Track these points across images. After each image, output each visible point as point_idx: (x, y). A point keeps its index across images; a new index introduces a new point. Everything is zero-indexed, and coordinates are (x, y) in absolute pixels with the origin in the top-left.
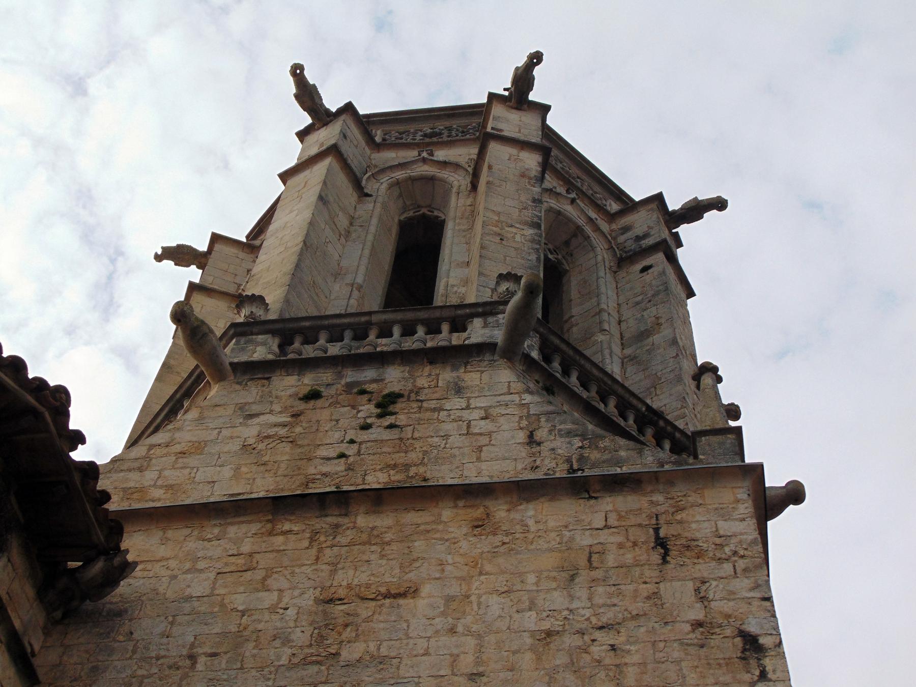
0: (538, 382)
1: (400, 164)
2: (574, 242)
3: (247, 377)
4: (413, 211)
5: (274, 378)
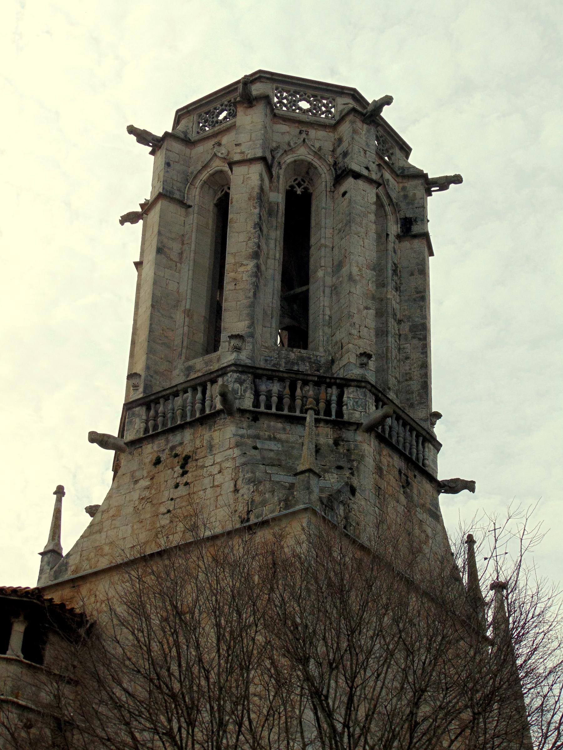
0: (248, 418)
1: (203, 167)
2: (311, 173)
3: (133, 448)
4: (220, 192)
5: (143, 447)
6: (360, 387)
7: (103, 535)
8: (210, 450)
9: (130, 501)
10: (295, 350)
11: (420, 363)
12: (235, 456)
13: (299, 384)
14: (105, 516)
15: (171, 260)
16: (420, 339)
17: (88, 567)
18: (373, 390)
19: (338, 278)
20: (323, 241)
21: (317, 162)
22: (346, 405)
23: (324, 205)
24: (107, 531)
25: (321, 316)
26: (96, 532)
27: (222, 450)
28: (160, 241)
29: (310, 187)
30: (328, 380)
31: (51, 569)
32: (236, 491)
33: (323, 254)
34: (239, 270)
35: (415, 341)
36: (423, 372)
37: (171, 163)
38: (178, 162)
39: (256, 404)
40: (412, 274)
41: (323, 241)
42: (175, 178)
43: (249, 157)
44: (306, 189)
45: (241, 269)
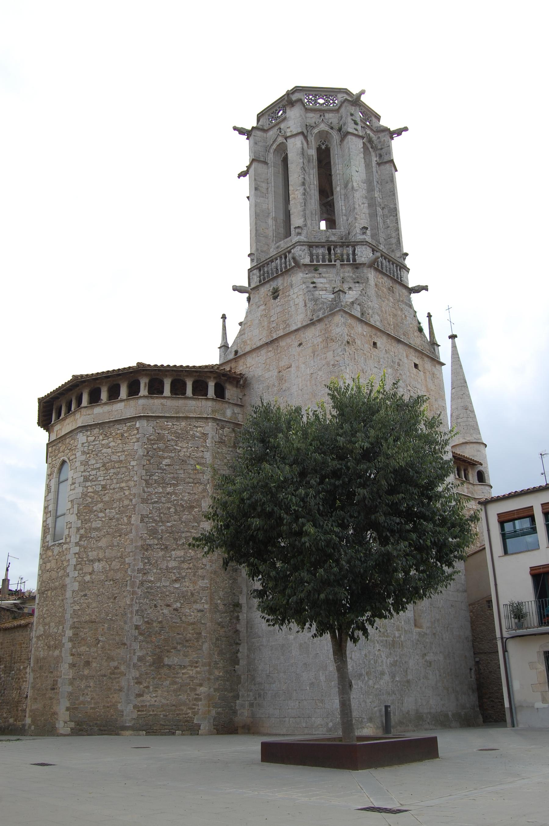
6: (363, 245)
7: (246, 335)
9: (256, 317)
14: (246, 326)
22: (357, 255)
23: (336, 153)
27: (297, 286)
32: (305, 306)
36: (397, 233)
40: (387, 183)
44: (327, 145)
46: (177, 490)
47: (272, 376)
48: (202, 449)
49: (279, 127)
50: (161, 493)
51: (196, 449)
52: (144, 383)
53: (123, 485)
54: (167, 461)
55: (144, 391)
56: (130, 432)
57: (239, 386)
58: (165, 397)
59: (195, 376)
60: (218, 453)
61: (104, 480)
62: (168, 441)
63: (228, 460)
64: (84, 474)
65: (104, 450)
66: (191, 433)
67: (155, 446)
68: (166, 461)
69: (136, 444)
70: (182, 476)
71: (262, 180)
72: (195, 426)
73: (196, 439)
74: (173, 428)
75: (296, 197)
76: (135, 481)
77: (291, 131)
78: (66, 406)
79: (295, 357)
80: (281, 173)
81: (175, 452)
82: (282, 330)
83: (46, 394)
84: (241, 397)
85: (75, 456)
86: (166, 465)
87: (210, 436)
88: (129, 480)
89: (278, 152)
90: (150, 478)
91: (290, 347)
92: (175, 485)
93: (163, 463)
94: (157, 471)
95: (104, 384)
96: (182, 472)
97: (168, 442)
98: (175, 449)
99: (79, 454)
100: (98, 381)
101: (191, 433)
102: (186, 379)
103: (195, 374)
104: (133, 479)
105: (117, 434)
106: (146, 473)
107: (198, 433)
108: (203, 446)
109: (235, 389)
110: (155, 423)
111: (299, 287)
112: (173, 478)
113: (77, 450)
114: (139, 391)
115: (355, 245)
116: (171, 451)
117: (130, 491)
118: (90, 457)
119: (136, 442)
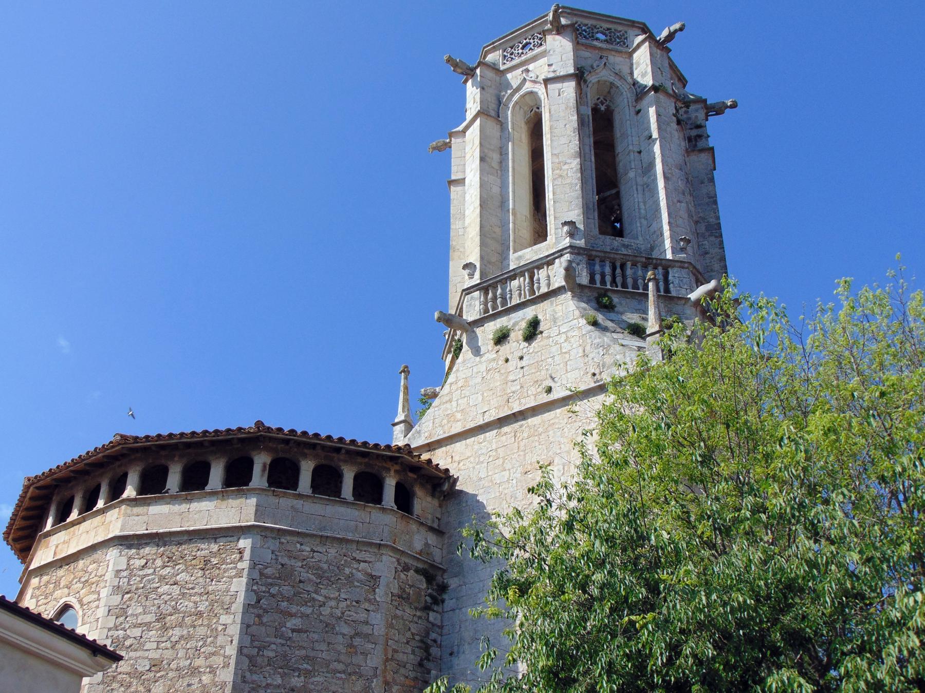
2: (612, 91)
6: (683, 268)
7: (454, 404)
8: (555, 322)
9: (477, 373)
10: (617, 238)
11: (719, 257)
12: (580, 325)
13: (629, 264)
14: (454, 387)
15: (493, 167)
16: (716, 237)
17: (442, 432)
18: (694, 271)
19: (649, 178)
20: (631, 147)
21: (618, 83)
22: (673, 283)
23: (628, 117)
24: (457, 400)
25: (637, 210)
26: (446, 402)
27: (566, 321)
28: (481, 151)
29: (611, 104)
30: (654, 261)
31: (405, 437)
32: (585, 355)
33: (632, 157)
34: (563, 168)
35: (712, 239)
36: (722, 264)
37: (485, 87)
38: (491, 87)
39: (592, 280)
40: (702, 183)
41: (631, 147)
42: (490, 100)
43: (562, 74)
44: (608, 106)
45: (566, 167)
46: (313, 683)
47: (508, 479)
48: (367, 605)
49: (524, 68)
50: (279, 686)
51: (354, 603)
52: (261, 461)
53: (199, 662)
54: (292, 623)
55: (258, 478)
56: (224, 556)
57: (437, 494)
58: (300, 496)
59: (361, 464)
60: (395, 617)
61: (158, 648)
62: (300, 581)
63: (413, 634)
64: (116, 633)
65: (165, 588)
66: (347, 571)
67: (274, 590)
68: (294, 622)
69: (234, 580)
70: (324, 655)
71: (492, 148)
72: (354, 559)
73: (356, 584)
74: (313, 557)
75: (564, 174)
76: (225, 657)
77: (554, 71)
78: (84, 497)
79: (562, 446)
80: (524, 141)
81: (313, 606)
82: (532, 397)
83: (62, 464)
84: (440, 517)
85: (96, 596)
86: (293, 631)
87: (383, 581)
88: (213, 654)
89: (520, 107)
90: (258, 653)
91: (550, 428)
92: (308, 674)
93: (289, 625)
94: (273, 640)
95: (176, 459)
96: (324, 647)
97: (301, 585)
98: (313, 598)
99: (104, 593)
100: (163, 453)
101: (347, 571)
102: (342, 468)
103: (360, 459)
104: (222, 652)
105: (195, 558)
106: (252, 641)
107: (359, 574)
108: (369, 601)
109: (429, 499)
110: (278, 544)
111: (570, 324)
112: (306, 658)
113: (102, 585)
114: (250, 479)
115: (669, 266)
116: (306, 602)
117: (215, 675)
118: (130, 599)
119: (235, 576)
